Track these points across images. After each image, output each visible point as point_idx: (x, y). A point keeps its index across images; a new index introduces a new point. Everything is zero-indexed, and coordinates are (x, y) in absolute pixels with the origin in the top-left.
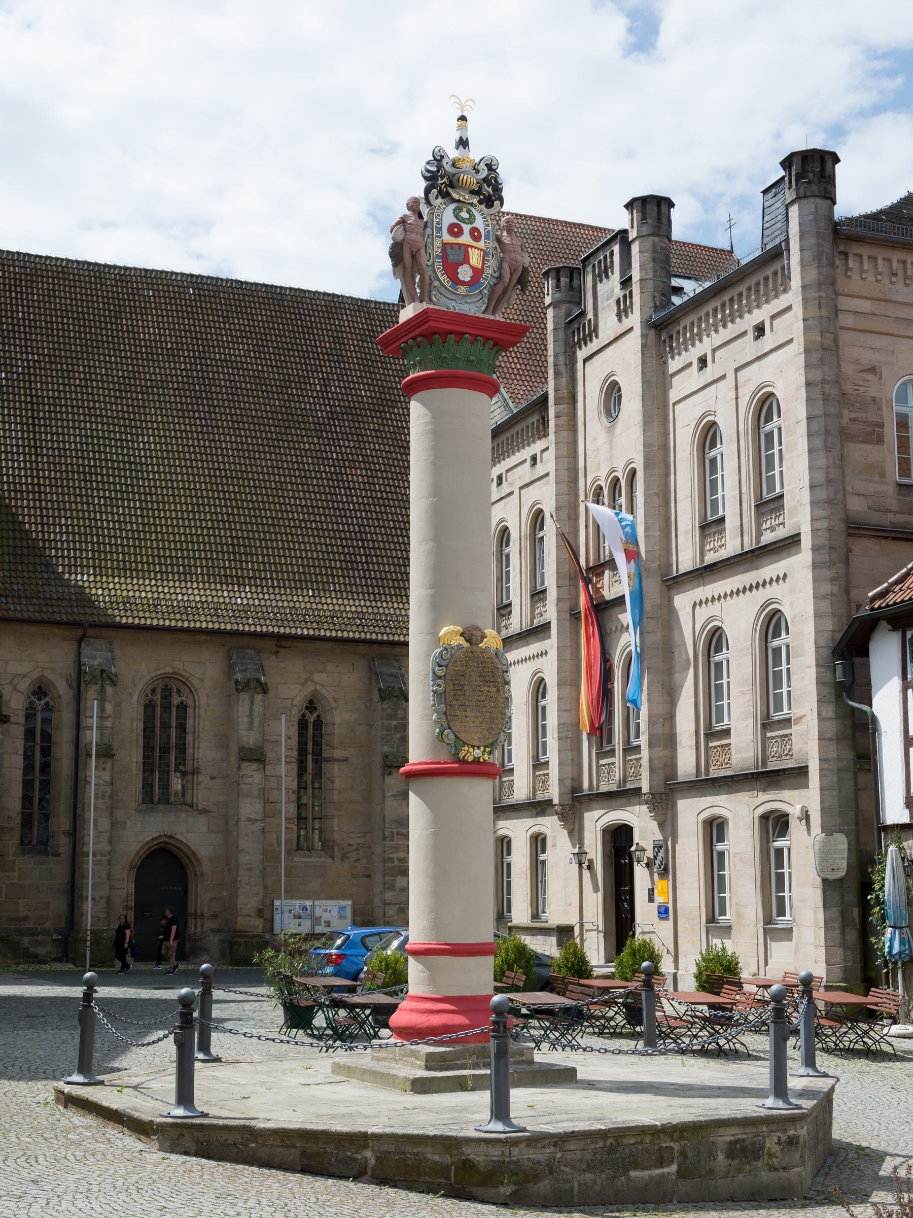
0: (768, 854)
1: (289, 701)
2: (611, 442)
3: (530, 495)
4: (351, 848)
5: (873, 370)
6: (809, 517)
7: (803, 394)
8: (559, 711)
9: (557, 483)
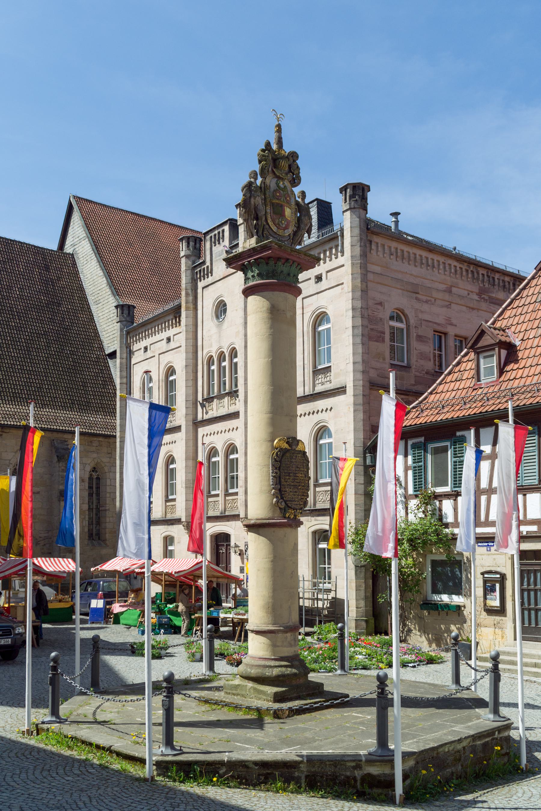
0: (316, 550)
1: (8, 461)
2: (220, 332)
3: (166, 359)
4: (42, 539)
5: (381, 304)
6: (352, 379)
7: (350, 313)
8: (186, 473)
9: (186, 352)
